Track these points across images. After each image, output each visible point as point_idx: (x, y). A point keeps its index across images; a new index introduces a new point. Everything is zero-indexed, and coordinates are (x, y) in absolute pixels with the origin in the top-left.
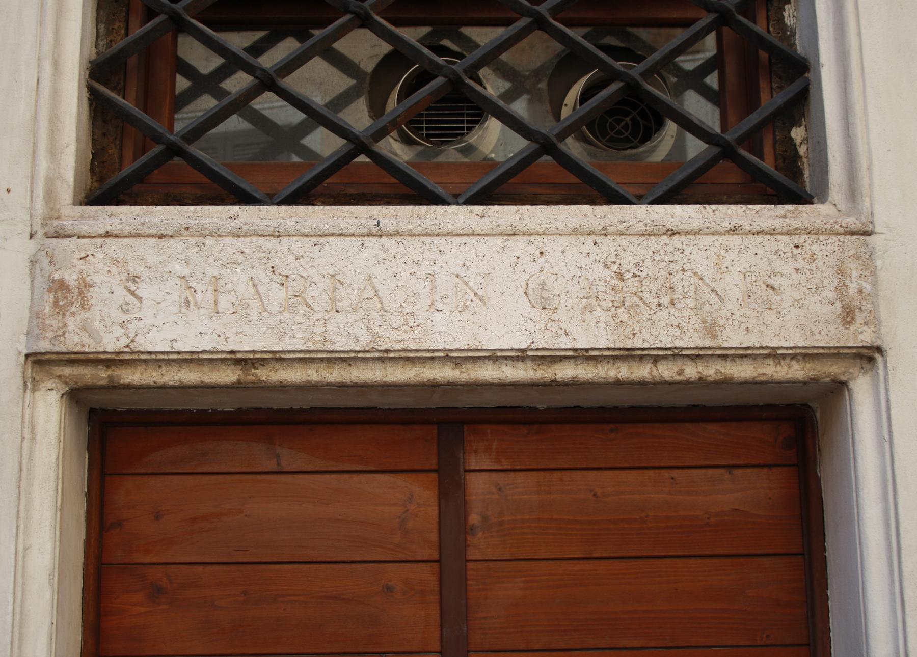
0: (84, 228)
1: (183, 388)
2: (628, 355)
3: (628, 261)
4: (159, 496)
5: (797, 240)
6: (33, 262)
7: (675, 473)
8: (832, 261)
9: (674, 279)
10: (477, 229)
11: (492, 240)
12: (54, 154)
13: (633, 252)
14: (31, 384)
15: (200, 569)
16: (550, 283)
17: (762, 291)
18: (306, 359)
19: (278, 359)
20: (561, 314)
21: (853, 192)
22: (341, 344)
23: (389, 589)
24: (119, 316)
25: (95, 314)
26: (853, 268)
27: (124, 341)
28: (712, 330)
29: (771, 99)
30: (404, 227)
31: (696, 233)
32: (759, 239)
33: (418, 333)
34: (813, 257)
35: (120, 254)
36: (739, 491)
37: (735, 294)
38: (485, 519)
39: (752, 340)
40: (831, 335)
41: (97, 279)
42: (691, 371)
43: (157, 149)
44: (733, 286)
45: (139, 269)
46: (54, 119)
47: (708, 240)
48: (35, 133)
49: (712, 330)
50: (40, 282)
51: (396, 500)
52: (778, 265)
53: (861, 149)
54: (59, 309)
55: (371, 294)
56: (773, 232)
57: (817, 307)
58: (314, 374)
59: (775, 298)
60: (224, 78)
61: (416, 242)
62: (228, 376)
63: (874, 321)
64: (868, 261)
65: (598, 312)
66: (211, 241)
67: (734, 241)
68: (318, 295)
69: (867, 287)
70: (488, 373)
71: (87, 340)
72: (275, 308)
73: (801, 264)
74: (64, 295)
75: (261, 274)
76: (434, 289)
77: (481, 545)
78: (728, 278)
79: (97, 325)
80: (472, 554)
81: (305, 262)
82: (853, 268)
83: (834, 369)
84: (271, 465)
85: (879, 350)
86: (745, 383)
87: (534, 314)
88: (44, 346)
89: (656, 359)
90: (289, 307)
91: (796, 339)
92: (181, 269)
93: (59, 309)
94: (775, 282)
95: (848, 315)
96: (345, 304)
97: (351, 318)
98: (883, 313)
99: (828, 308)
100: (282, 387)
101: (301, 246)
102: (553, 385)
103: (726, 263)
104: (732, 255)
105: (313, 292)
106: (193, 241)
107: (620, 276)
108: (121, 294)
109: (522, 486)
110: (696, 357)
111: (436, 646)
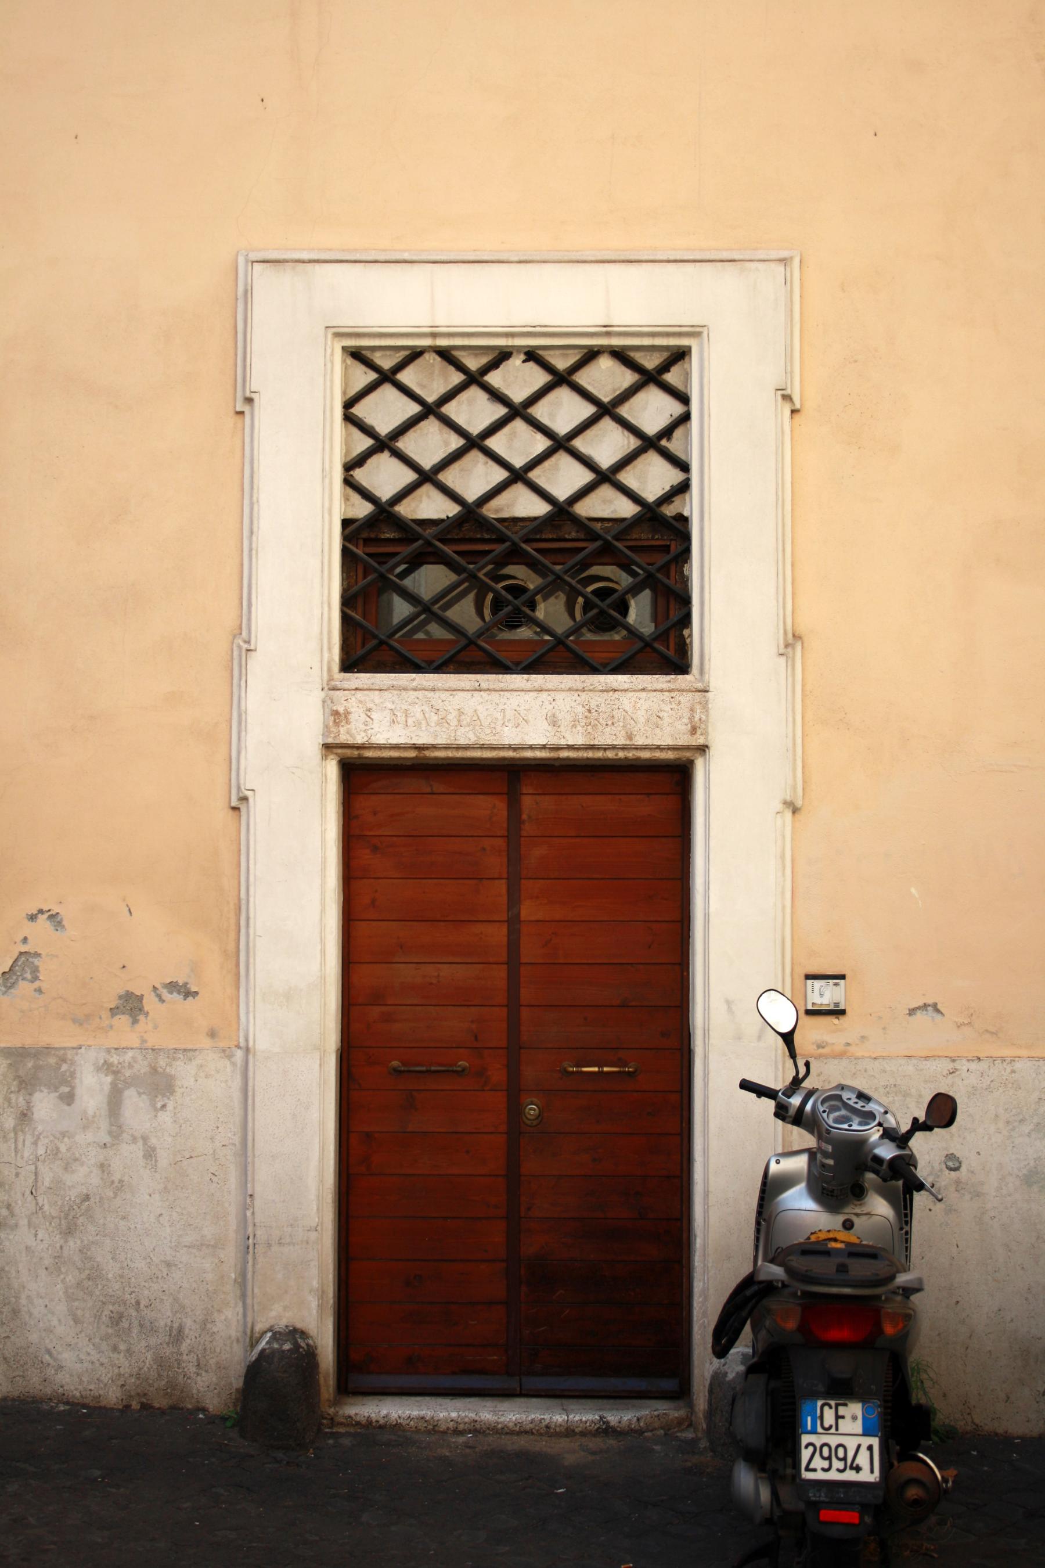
0: (346, 685)
1: (391, 759)
2: (592, 747)
3: (593, 704)
4: (364, 803)
5: (673, 694)
6: (324, 702)
7: (622, 797)
8: (688, 705)
9: (614, 713)
10: (525, 688)
11: (531, 694)
12: (330, 649)
13: (596, 700)
14: (325, 757)
15: (395, 839)
16: (557, 714)
17: (654, 719)
18: (447, 748)
19: (434, 747)
20: (562, 729)
21: (702, 671)
22: (462, 741)
23: (484, 849)
24: (363, 727)
25: (352, 726)
26: (698, 709)
27: (366, 739)
28: (630, 737)
29: (675, 615)
30: (491, 687)
31: (626, 691)
32: (655, 694)
33: (497, 737)
34: (679, 703)
35: (362, 699)
36: (643, 807)
37: (642, 720)
38: (529, 817)
39: (648, 742)
40: (684, 740)
41: (353, 710)
42: (621, 754)
43: (375, 642)
44: (641, 716)
45: (371, 705)
46: (330, 632)
47: (630, 694)
48: (321, 640)
49: (630, 737)
50: (327, 711)
51: (488, 807)
52: (663, 706)
53: (706, 651)
54: (336, 724)
55: (475, 718)
56: (662, 691)
57: (679, 727)
58: (450, 754)
59: (660, 722)
60: (400, 596)
61: (497, 694)
62: (412, 754)
63: (705, 734)
64: (705, 705)
65: (579, 728)
66: (404, 693)
67: (643, 694)
68: (452, 717)
69: (704, 717)
70: (529, 754)
71: (349, 738)
72: (433, 724)
73: (674, 706)
74: (338, 717)
75: (426, 708)
76: (504, 716)
77: (528, 829)
78: (639, 712)
79: (354, 731)
80: (524, 833)
81: (446, 703)
82: (698, 709)
83: (688, 754)
84: (429, 790)
85: (707, 746)
86: (646, 760)
87: (550, 728)
88: (330, 740)
89: (605, 749)
90: (439, 724)
91: (669, 741)
92: (390, 706)
93: (336, 724)
94: (661, 714)
95: (694, 731)
96: (464, 723)
97: (467, 729)
98: (710, 729)
99: (684, 727)
100: (436, 758)
101: (445, 695)
102: (559, 759)
103: (639, 705)
104: (641, 702)
105: (450, 717)
106: (396, 692)
107: (589, 711)
108: (363, 717)
109: (547, 802)
110: (624, 748)
111: (505, 875)
